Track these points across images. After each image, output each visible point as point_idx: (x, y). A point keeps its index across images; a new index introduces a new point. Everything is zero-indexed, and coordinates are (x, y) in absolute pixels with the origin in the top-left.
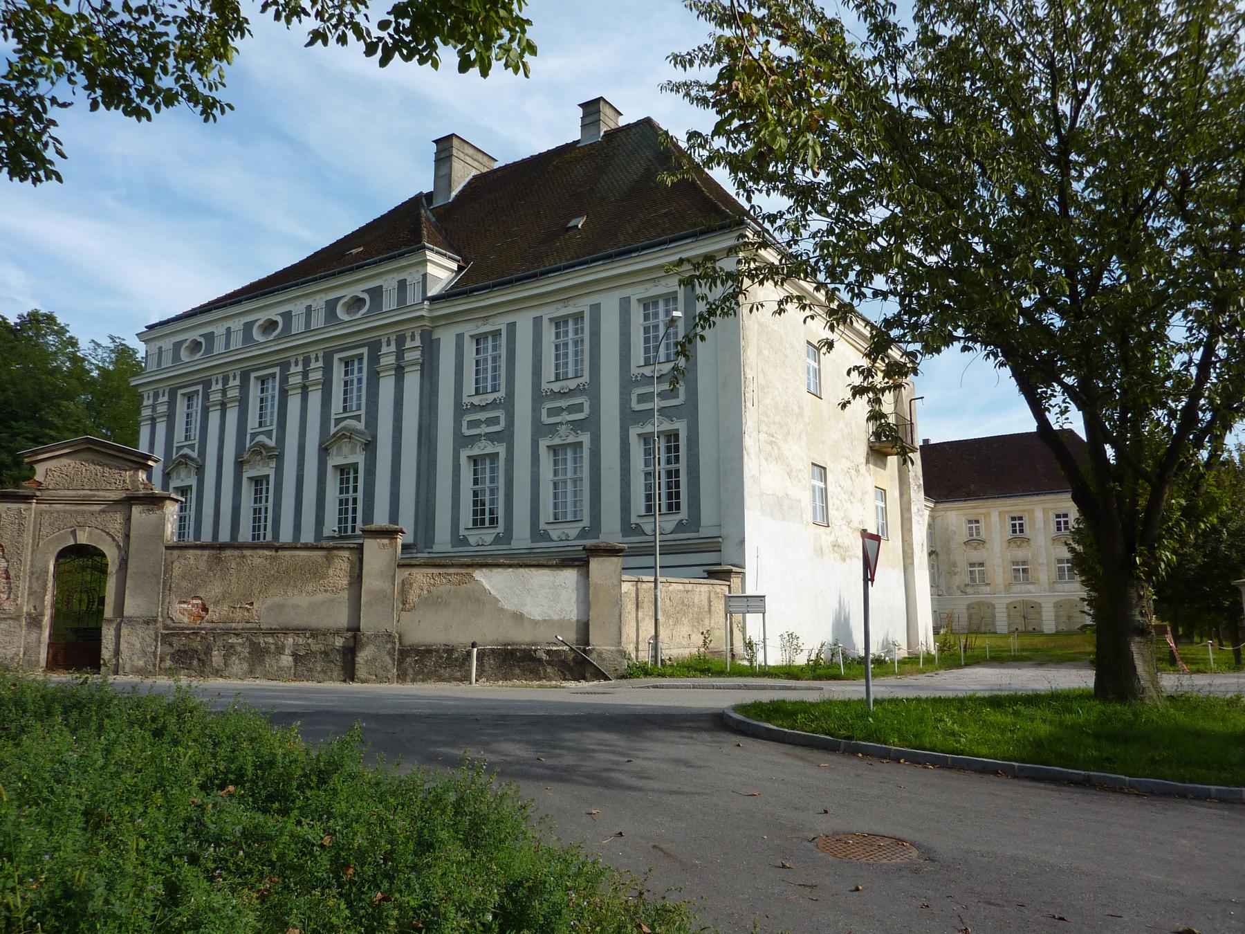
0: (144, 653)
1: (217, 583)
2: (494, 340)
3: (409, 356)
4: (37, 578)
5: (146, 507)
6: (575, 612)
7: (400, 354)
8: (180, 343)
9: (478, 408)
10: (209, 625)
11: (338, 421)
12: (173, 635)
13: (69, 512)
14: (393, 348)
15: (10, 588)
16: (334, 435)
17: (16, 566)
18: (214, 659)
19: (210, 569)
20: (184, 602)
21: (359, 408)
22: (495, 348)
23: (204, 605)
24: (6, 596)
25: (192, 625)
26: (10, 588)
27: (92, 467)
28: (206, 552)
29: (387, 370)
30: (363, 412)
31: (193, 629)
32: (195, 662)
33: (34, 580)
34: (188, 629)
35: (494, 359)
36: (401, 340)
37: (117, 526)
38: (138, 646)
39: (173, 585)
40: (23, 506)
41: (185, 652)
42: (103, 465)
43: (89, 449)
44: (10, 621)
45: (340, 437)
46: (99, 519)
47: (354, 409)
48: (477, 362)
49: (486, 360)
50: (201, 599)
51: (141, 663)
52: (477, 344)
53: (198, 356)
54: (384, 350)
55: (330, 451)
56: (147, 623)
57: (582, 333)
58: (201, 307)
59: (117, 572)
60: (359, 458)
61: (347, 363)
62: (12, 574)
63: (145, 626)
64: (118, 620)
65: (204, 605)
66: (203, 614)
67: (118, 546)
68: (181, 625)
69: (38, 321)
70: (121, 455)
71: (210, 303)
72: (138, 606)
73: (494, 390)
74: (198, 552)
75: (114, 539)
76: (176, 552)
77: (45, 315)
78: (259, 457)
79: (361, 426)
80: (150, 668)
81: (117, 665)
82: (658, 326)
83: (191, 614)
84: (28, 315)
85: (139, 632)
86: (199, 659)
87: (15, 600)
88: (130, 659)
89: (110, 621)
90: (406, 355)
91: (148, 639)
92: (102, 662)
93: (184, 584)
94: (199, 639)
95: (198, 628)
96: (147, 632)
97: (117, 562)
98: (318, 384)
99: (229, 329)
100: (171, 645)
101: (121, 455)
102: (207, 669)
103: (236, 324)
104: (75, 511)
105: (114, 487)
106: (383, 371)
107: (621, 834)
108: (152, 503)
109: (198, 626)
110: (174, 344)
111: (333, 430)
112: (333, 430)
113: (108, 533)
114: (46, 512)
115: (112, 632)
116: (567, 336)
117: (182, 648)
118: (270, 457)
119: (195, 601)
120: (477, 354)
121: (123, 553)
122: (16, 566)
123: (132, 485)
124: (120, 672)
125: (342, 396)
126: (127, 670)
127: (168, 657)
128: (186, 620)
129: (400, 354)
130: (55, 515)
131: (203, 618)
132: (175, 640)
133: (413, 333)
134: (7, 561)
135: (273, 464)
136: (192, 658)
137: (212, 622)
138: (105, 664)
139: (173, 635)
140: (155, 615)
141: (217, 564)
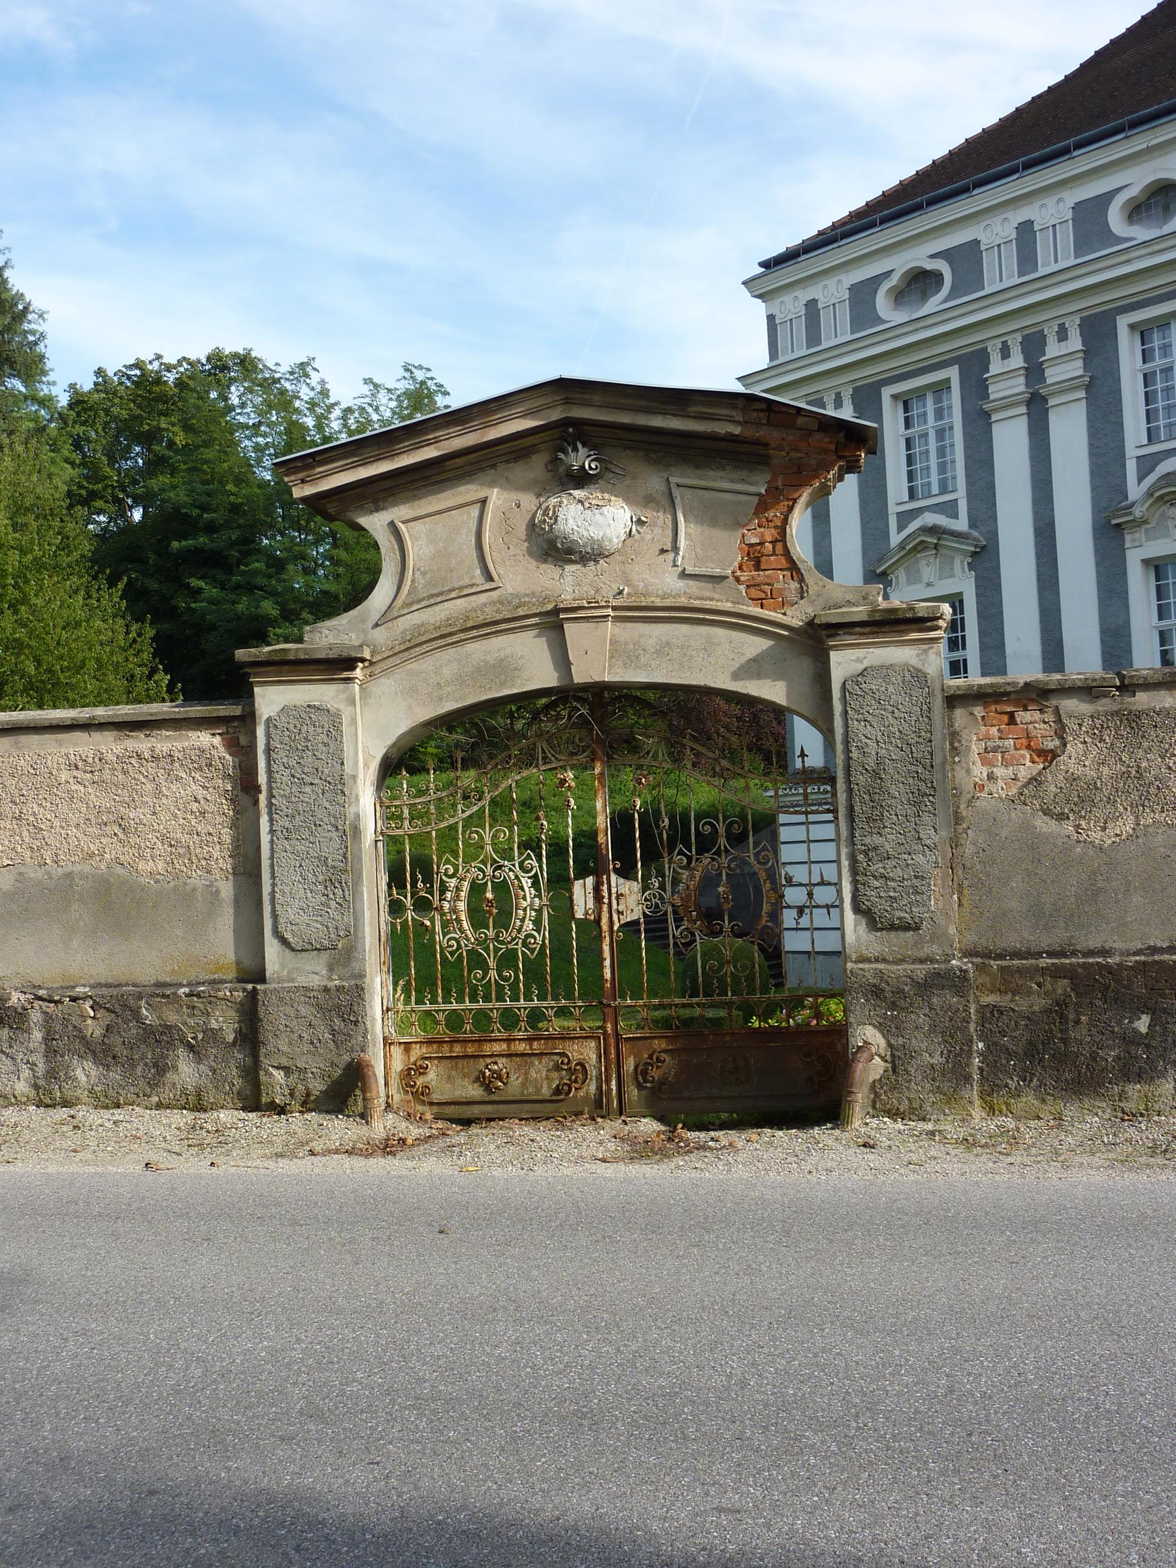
2: (938, 400)
3: (1054, 375)
6: (231, 947)
7: (1034, 371)
8: (874, 282)
11: (905, 518)
14: (1017, 360)
16: (902, 546)
22: (939, 414)
29: (1062, 392)
30: (960, 494)
35: (940, 434)
36: (1034, 344)
45: (914, 548)
47: (935, 490)
48: (908, 441)
49: (925, 435)
52: (906, 410)
53: (933, 304)
54: (996, 366)
55: (892, 577)
57: (950, 415)
58: (834, 226)
60: (966, 585)
61: (906, 402)
69: (225, 368)
71: (855, 216)
73: (944, 490)
77: (235, 355)
79: (961, 524)
82: (926, 435)
84: (209, 359)
90: (1047, 373)
98: (1076, 388)
99: (812, 305)
103: (998, 229)
106: (996, 410)
107: (441, 1232)
110: (853, 289)
111: (895, 539)
112: (895, 539)
116: (925, 423)
120: (907, 426)
125: (904, 469)
129: (1034, 371)
133: (1062, 326)
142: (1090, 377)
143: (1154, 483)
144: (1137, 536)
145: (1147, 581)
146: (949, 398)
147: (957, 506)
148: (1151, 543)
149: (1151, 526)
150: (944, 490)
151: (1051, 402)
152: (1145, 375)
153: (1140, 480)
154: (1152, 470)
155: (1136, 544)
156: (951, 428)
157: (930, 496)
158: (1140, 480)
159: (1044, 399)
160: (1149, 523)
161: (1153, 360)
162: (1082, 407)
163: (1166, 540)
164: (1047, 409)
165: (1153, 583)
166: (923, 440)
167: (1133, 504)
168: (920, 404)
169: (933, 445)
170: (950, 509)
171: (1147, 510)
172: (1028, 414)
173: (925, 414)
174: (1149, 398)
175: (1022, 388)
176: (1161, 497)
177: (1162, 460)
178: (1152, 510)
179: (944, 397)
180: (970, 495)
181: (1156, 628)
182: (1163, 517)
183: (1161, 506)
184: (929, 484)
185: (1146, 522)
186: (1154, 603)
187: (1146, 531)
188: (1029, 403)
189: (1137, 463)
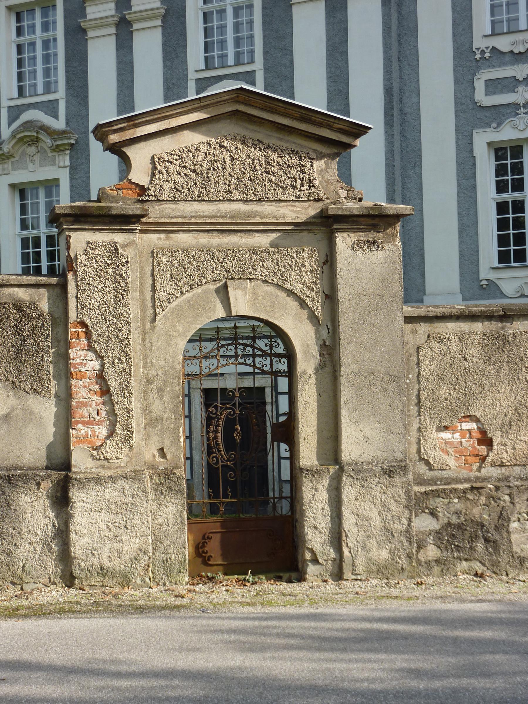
0: (389, 532)
1: (505, 388)
4: (161, 391)
5: (362, 236)
9: (508, 58)
10: (495, 472)
12: (436, 494)
13: (210, 252)
15: (112, 413)
17: (119, 367)
18: (514, 537)
19: (489, 361)
20: (446, 428)
21: (48, 89)
22: (46, 27)
23: (483, 432)
24: (103, 432)
25: (464, 473)
26: (112, 413)
27: (243, 152)
28: (478, 327)
31: (467, 480)
32: (480, 546)
33: (153, 394)
34: (458, 481)
35: (46, 44)
37: (307, 278)
38: (377, 521)
39: (424, 395)
40: (119, 238)
41: (460, 527)
42: (257, 144)
43: (236, 114)
44: (123, 483)
46: (269, 264)
47: (231, 61)
49: (33, 44)
50: (477, 420)
51: (384, 554)
56: (389, 473)
57: (55, 29)
59: (317, 370)
62: (113, 383)
63: (385, 480)
64: (332, 469)
65: (483, 432)
66: (483, 450)
67: (313, 318)
68: (445, 474)
70: (303, 126)
72: (367, 440)
74: (463, 326)
75: (302, 304)
76: (423, 328)
78: (32, 150)
80: (403, 562)
81: (339, 562)
82: (224, 11)
83: (460, 452)
85: (377, 492)
86: (487, 540)
87: (127, 438)
88: (364, 547)
89: (313, 473)
90: (89, 10)
91: (393, 506)
92: (308, 556)
93: (444, 391)
94: (483, 499)
95: (477, 479)
96: (391, 491)
97: (315, 350)
100: (433, 514)
101: (303, 126)
102: (504, 558)
104: (221, 249)
105: (291, 194)
108: (375, 228)
109: (473, 474)
113: (290, 293)
114: (162, 250)
115: (323, 495)
116: (34, 32)
117: (454, 520)
118: (57, 149)
119: (466, 426)
121: (324, 332)
122: (119, 367)
123: (326, 190)
124: (348, 574)
126: (360, 568)
127: (431, 539)
128: (452, 462)
130: (180, 256)
131: (483, 459)
132: (439, 503)
134: (100, 357)
135: (65, 160)
136: (473, 538)
137: (502, 465)
138: (315, 561)
139: (436, 494)
140: (400, 456)
141: (501, 349)
142: (166, 10)
143: (17, 129)
144: (6, 166)
145: (13, 201)
146: (55, 15)
147: (58, 103)
148: (16, 172)
149: (16, 159)
150: (48, 90)
151: (135, 26)
152: (205, 14)
153: (10, 124)
154: (17, 118)
155: (5, 172)
156: (55, 40)
157: (36, 95)
158: (10, 124)
159: (129, 24)
160: (14, 157)
161: (24, 35)
162: (158, 33)
163: (51, 168)
164: (86, 40)
165: (18, 202)
166: (31, 47)
167: (3, 141)
168: (30, 17)
169: (39, 53)
170: (250, 77)
171: (12, 147)
172: (162, 27)
173: (33, 26)
174: (207, 32)
175: (113, 12)
176: (21, 139)
177: (24, 111)
178: (16, 148)
179: (51, 13)
180: (267, 69)
181: (19, 235)
182: (24, 154)
183: (21, 146)
184: (35, 85)
185: (12, 156)
186: (18, 217)
187: (12, 162)
188: (118, 25)
189: (8, 111)
